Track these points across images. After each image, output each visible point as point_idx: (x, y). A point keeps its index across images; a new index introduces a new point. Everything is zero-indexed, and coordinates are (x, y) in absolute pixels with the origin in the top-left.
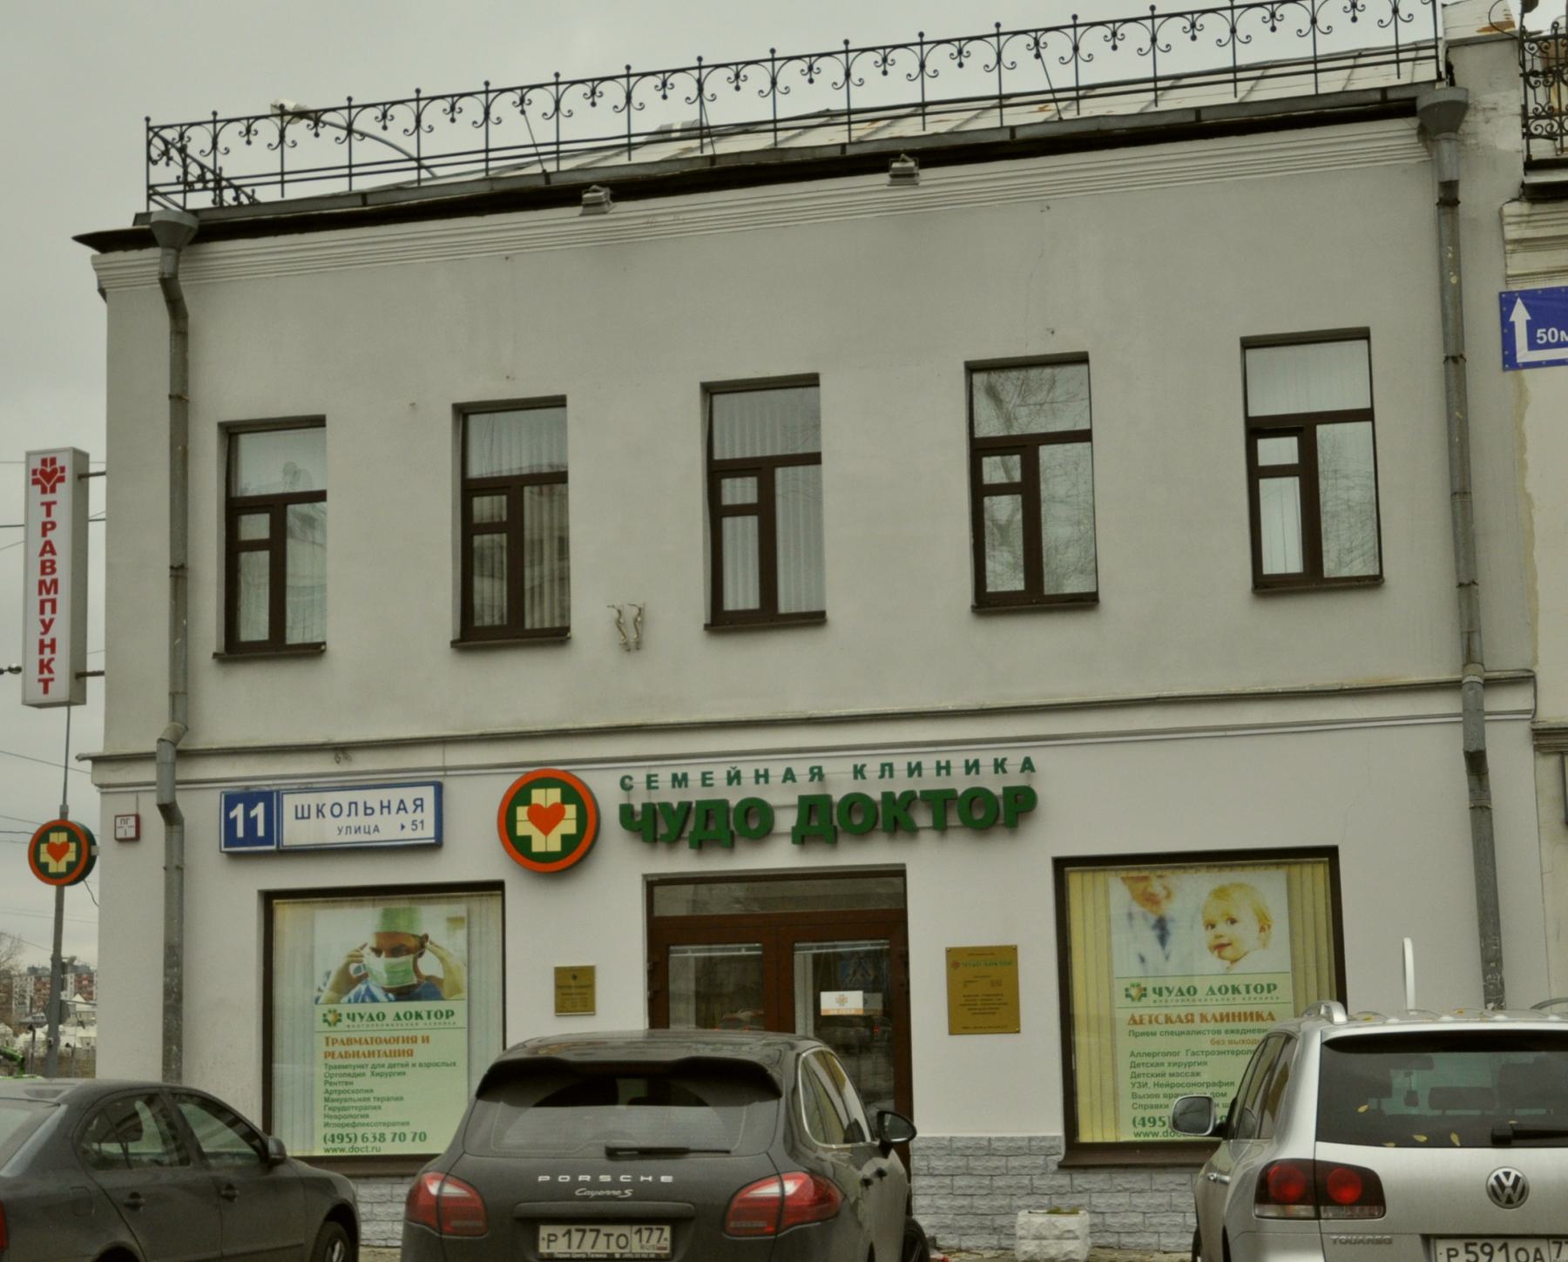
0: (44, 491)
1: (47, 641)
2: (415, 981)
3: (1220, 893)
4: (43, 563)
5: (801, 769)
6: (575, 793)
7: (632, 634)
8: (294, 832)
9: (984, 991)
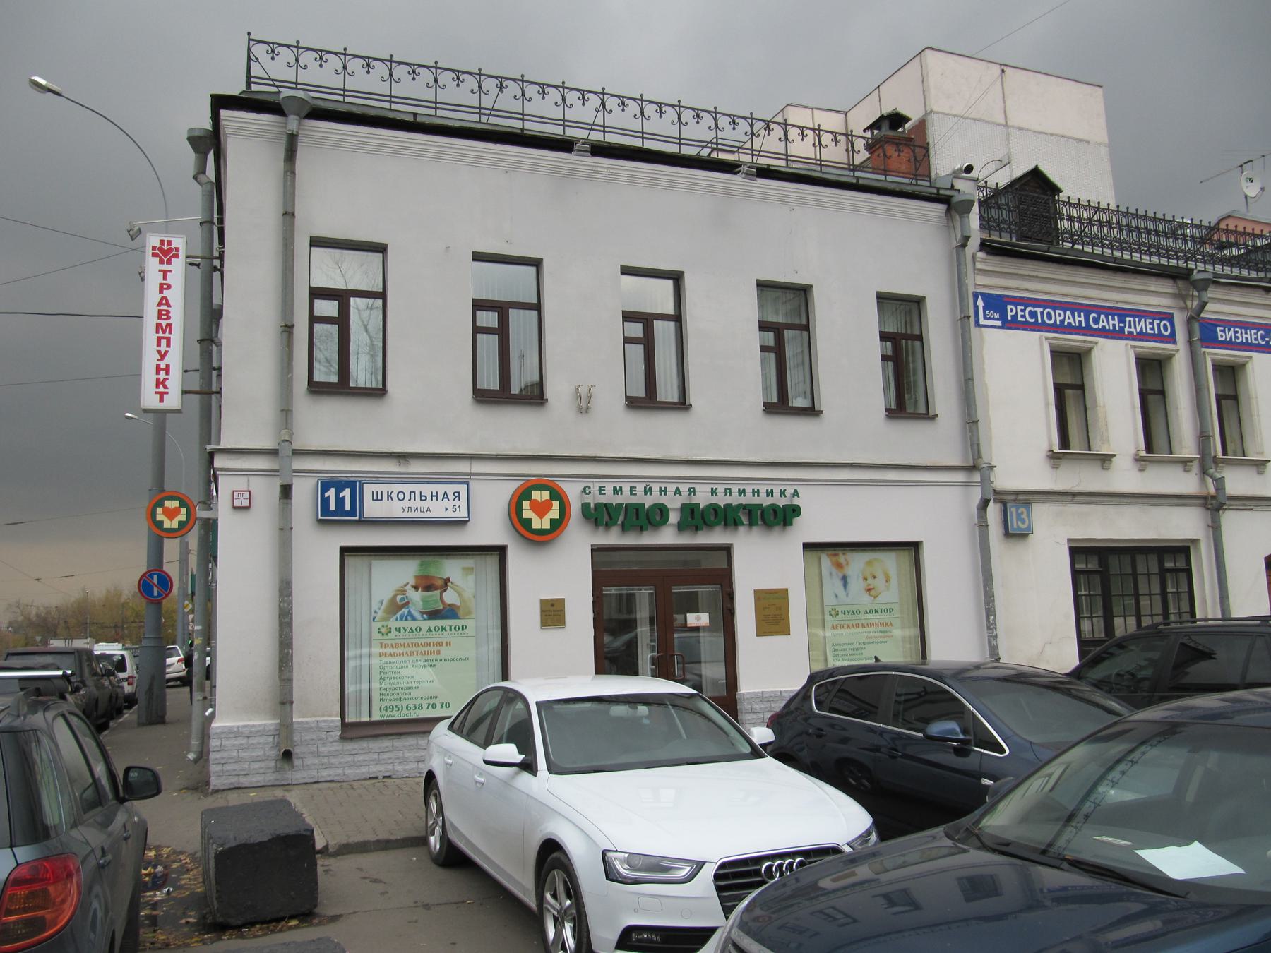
0: (161, 262)
1: (163, 366)
2: (441, 607)
3: (869, 563)
4: (160, 312)
5: (684, 488)
6: (557, 495)
7: (583, 404)
8: (371, 509)
9: (773, 613)
